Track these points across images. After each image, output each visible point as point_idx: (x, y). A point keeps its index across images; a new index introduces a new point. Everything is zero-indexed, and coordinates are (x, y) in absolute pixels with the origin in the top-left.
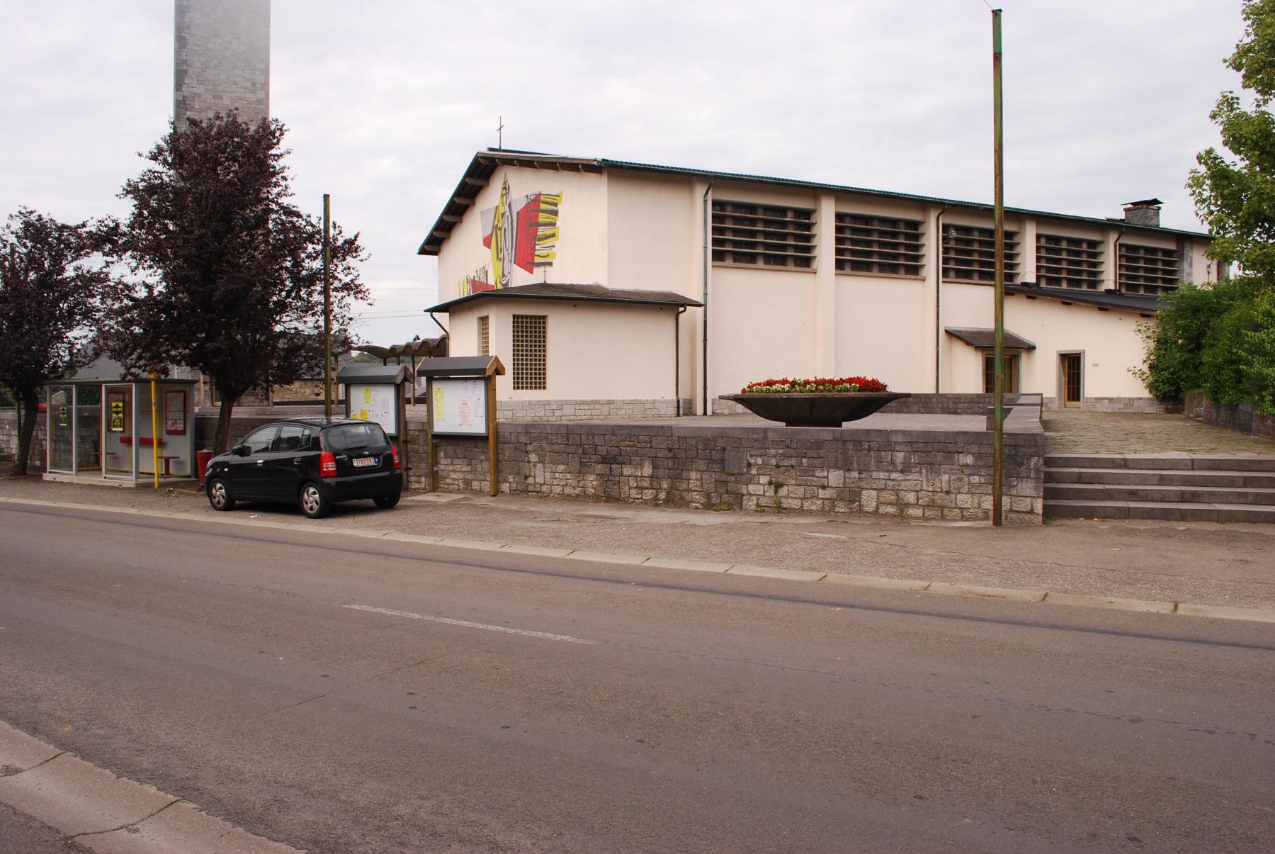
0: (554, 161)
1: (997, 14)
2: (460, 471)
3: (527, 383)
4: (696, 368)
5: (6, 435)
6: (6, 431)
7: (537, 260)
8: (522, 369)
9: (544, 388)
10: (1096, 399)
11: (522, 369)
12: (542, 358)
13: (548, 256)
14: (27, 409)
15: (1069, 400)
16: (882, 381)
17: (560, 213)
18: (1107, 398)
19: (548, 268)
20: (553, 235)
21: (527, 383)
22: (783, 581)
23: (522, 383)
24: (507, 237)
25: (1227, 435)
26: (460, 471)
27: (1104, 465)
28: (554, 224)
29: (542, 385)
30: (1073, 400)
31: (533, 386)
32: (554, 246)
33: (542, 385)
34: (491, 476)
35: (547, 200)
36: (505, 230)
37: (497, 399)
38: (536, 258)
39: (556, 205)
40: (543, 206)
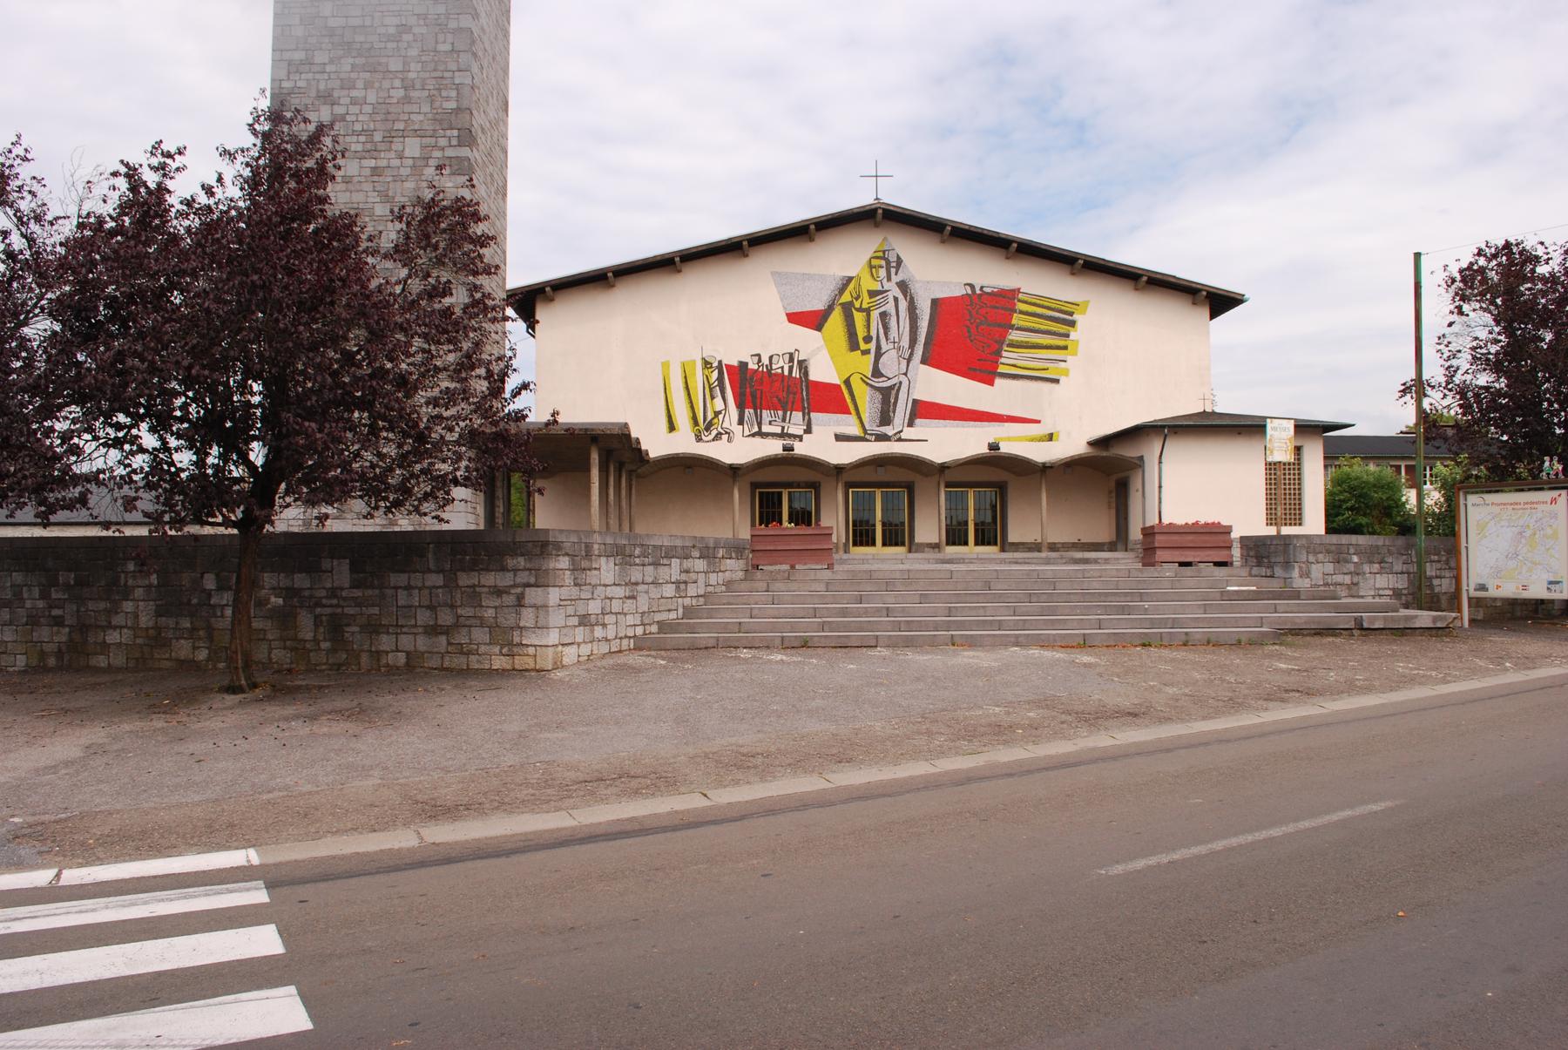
0: (1140, 272)
1: (1417, 256)
2: (620, 651)
5: (1351, 573)
6: (1351, 567)
7: (1002, 369)
9: (1300, 524)
12: (1297, 497)
14: (514, 554)
16: (1224, 523)
17: (1078, 325)
19: (1053, 385)
20: (1065, 348)
22: (87, 864)
26: (620, 651)
28: (1067, 336)
31: (1288, 522)
35: (1026, 299)
38: (1001, 366)
40: (1021, 306)
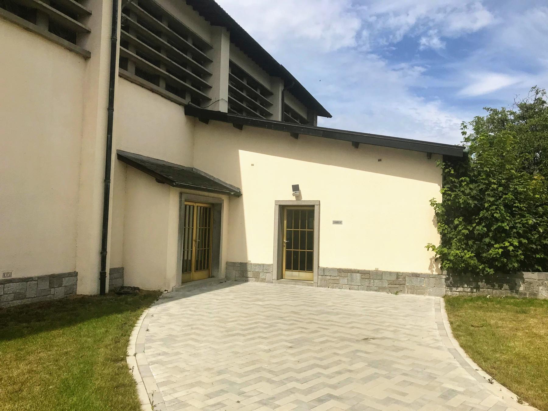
10: (340, 271)
15: (288, 268)
18: (358, 272)
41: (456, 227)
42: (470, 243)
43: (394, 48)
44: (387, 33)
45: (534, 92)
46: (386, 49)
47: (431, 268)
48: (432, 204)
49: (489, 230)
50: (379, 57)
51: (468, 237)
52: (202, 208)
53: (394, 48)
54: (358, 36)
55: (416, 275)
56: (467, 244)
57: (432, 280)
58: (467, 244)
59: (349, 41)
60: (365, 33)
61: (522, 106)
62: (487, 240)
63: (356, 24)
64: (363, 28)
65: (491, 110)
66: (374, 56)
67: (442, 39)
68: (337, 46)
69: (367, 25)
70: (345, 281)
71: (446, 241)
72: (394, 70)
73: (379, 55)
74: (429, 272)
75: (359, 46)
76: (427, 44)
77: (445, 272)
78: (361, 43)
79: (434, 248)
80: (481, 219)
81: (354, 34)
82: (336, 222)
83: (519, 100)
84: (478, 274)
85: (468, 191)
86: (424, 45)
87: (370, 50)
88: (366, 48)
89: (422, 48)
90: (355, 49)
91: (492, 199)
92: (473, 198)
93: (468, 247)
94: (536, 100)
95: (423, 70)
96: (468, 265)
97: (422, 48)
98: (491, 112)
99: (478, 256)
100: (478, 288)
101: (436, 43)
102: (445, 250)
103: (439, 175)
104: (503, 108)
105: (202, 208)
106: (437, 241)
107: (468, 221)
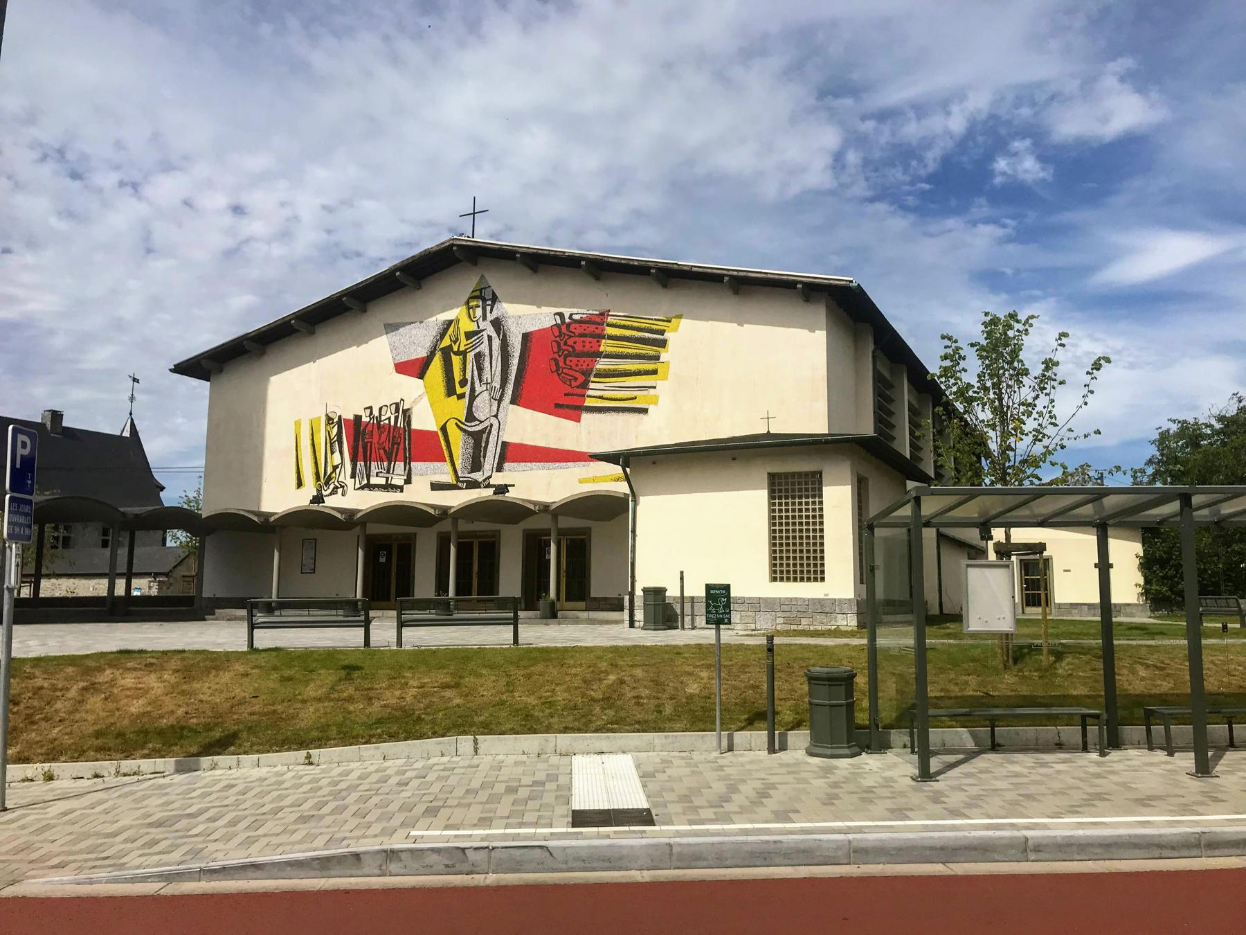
3: (809, 572)
4: (469, 532)
7: (589, 402)
8: (808, 558)
10: (1071, 604)
11: (808, 558)
13: (636, 398)
15: (1028, 605)
18: (1085, 604)
20: (655, 372)
21: (809, 572)
23: (802, 572)
24: (494, 364)
25: (103, 874)
27: (1241, 811)
28: (657, 358)
29: (819, 576)
30: (1034, 605)
32: (655, 387)
33: (819, 576)
34: (1171, 689)
36: (479, 356)
37: (732, 595)
39: (662, 332)
41: (1155, 572)
42: (1165, 581)
43: (926, 187)
44: (905, 154)
45: (1236, 400)
46: (907, 188)
47: (1138, 599)
48: (1137, 557)
49: (1177, 573)
50: (892, 208)
51: (1163, 578)
52: (510, 582)
53: (926, 187)
54: (838, 160)
55: (1129, 605)
56: (1163, 583)
57: (1140, 608)
58: (1163, 583)
59: (817, 175)
60: (852, 157)
61: (1221, 419)
62: (1176, 579)
63: (830, 138)
64: (846, 145)
65: (1179, 422)
66: (881, 207)
67: (1042, 159)
68: (794, 190)
69: (856, 140)
70: (1076, 611)
71: (1147, 581)
72: (931, 235)
73: (892, 204)
74: (1137, 602)
75: (843, 186)
76: (1010, 172)
77: (1149, 602)
78: (845, 179)
79: (1140, 585)
80: (1171, 566)
81: (829, 160)
82: (1065, 571)
83: (1216, 412)
84: (1171, 601)
85: (1161, 548)
86: (1004, 173)
87: (869, 194)
88: (860, 189)
89: (998, 180)
90: (831, 193)
91: (1177, 553)
92: (1165, 552)
93: (1164, 584)
94: (1238, 409)
95: (999, 232)
96: (1164, 595)
97: (998, 180)
98: (1180, 425)
99: (1171, 589)
100: (1172, 611)
101: (1029, 168)
102: (1148, 587)
103: (1139, 535)
104: (1195, 419)
105: (510, 582)
106: (1141, 581)
107: (1162, 567)
